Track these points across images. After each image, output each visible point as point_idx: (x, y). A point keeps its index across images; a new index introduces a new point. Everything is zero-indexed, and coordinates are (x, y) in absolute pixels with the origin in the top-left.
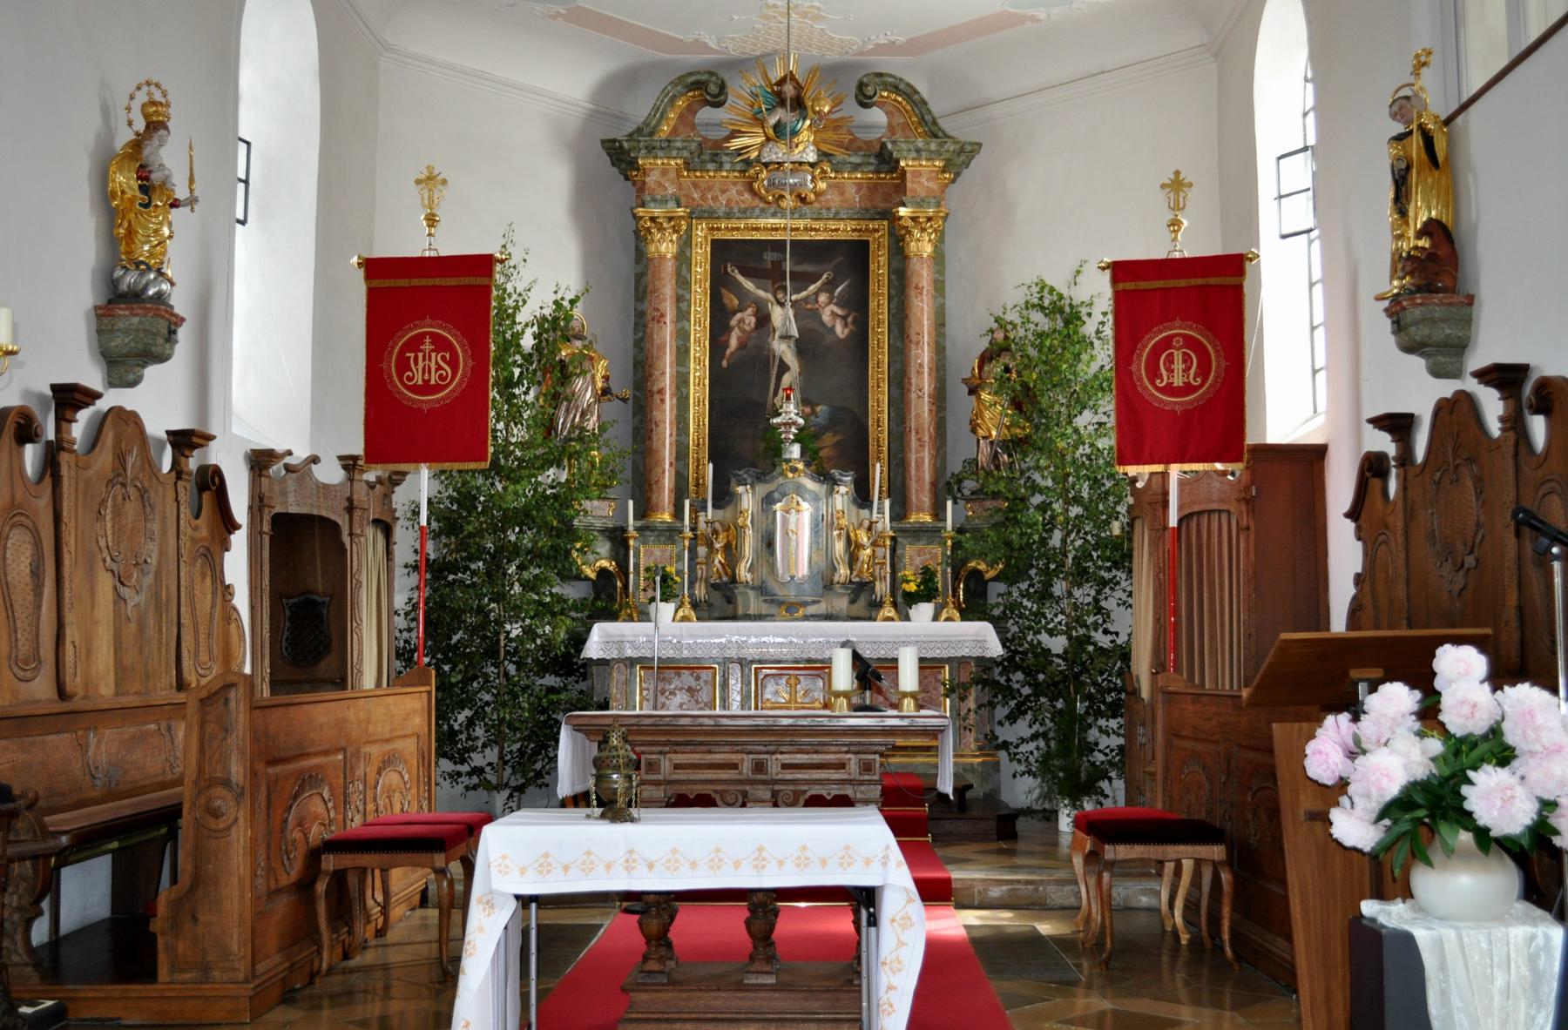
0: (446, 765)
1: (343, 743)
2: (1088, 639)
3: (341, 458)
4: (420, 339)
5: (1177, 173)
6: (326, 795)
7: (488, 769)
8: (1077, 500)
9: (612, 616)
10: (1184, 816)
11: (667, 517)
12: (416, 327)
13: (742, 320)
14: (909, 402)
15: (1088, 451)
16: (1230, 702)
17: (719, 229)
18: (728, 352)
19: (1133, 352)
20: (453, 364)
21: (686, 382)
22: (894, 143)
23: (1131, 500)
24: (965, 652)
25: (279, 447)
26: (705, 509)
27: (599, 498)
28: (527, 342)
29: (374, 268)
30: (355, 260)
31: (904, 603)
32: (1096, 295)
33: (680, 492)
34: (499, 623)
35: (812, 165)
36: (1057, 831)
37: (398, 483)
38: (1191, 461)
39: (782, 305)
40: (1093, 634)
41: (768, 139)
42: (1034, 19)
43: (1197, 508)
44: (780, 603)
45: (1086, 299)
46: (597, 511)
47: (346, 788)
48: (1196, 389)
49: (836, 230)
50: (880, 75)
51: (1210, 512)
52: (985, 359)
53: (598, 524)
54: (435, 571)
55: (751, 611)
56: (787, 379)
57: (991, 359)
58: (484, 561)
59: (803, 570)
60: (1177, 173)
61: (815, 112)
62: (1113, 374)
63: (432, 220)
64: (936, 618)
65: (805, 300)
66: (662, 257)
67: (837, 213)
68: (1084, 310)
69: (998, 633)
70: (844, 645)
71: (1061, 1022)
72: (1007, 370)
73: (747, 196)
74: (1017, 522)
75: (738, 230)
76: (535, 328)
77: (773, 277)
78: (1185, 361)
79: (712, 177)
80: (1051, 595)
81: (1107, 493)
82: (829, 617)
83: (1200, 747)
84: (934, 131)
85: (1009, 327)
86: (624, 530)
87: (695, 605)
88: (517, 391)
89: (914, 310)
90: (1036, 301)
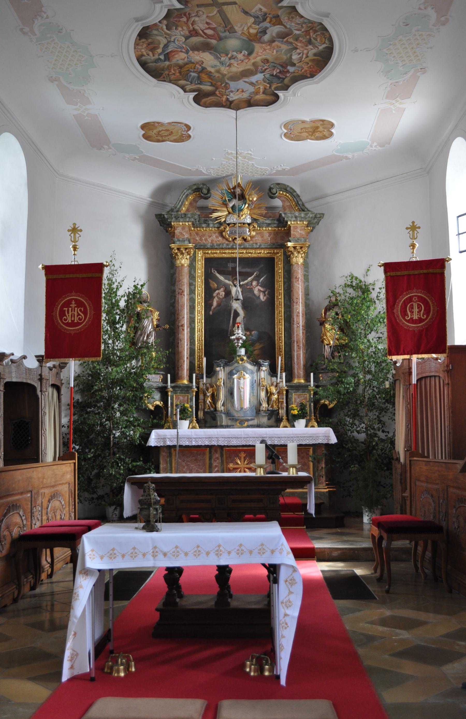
0: (86, 495)
1: (30, 489)
2: (376, 435)
3: (36, 356)
4: (69, 302)
5: (413, 222)
6: (21, 513)
7: (106, 496)
8: (369, 372)
9: (161, 427)
10: (422, 519)
11: (186, 382)
12: (68, 296)
13: (219, 294)
14: (294, 329)
15: (374, 350)
16: (444, 465)
17: (208, 253)
18: (212, 308)
19: (394, 305)
20: (85, 313)
21: (194, 321)
22: (285, 214)
23: (394, 372)
24: (320, 441)
25: (7, 352)
26: (202, 378)
27: (155, 373)
28: (122, 304)
29: (50, 270)
30: (40, 266)
31: (291, 420)
32: (377, 279)
33: (192, 370)
34: (110, 430)
35: (249, 224)
36: (362, 522)
37: (63, 367)
38: (422, 353)
39: (235, 286)
40: (378, 432)
41: (229, 213)
42: (347, 158)
43: (424, 375)
44: (236, 420)
45: (372, 282)
46: (154, 379)
47: (32, 509)
48: (424, 320)
49: (260, 253)
50: (278, 184)
51: (430, 377)
52: (327, 309)
53: (155, 385)
54: (78, 408)
55: (224, 424)
56: (239, 319)
57: (329, 310)
58: (104, 402)
59: (247, 405)
60: (413, 222)
61: (250, 201)
62: (385, 316)
63: (75, 248)
64: (306, 426)
65: (247, 284)
66: (183, 265)
67: (260, 245)
68: (371, 287)
69: (334, 432)
70: (263, 442)
71: (368, 623)
72: (337, 314)
73: (220, 238)
74: (342, 383)
75: (218, 254)
76: (126, 298)
77: (231, 274)
78: (418, 308)
79: (204, 229)
80: (358, 415)
81: (383, 369)
82: (258, 426)
83: (430, 486)
84: (302, 208)
85: (337, 295)
86: (166, 387)
87: (198, 421)
88: (118, 326)
89: (295, 288)
90: (349, 283)
